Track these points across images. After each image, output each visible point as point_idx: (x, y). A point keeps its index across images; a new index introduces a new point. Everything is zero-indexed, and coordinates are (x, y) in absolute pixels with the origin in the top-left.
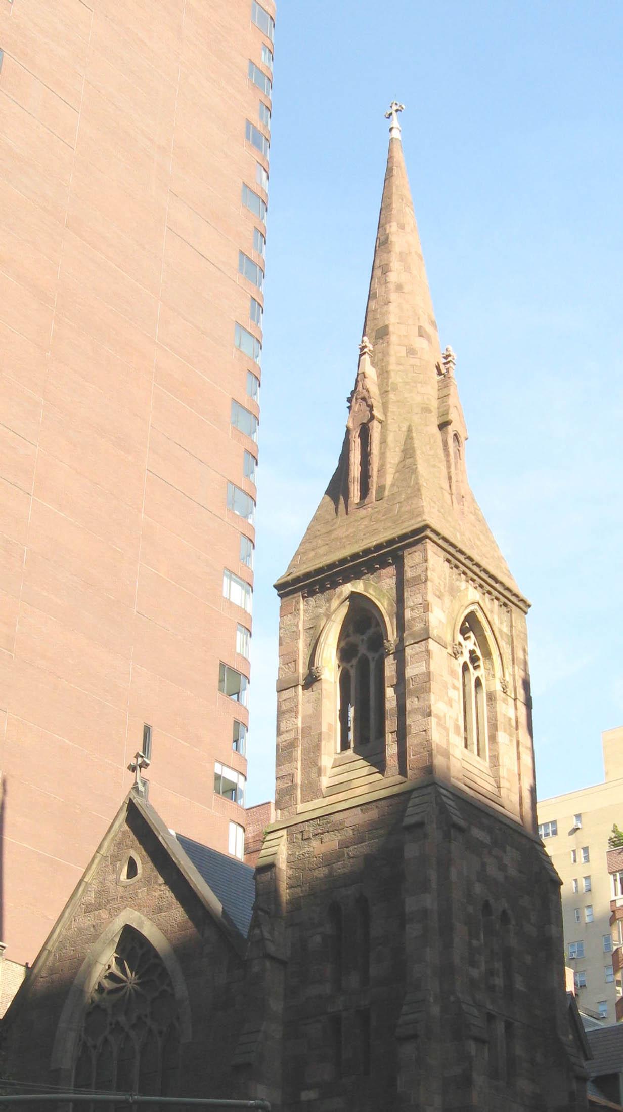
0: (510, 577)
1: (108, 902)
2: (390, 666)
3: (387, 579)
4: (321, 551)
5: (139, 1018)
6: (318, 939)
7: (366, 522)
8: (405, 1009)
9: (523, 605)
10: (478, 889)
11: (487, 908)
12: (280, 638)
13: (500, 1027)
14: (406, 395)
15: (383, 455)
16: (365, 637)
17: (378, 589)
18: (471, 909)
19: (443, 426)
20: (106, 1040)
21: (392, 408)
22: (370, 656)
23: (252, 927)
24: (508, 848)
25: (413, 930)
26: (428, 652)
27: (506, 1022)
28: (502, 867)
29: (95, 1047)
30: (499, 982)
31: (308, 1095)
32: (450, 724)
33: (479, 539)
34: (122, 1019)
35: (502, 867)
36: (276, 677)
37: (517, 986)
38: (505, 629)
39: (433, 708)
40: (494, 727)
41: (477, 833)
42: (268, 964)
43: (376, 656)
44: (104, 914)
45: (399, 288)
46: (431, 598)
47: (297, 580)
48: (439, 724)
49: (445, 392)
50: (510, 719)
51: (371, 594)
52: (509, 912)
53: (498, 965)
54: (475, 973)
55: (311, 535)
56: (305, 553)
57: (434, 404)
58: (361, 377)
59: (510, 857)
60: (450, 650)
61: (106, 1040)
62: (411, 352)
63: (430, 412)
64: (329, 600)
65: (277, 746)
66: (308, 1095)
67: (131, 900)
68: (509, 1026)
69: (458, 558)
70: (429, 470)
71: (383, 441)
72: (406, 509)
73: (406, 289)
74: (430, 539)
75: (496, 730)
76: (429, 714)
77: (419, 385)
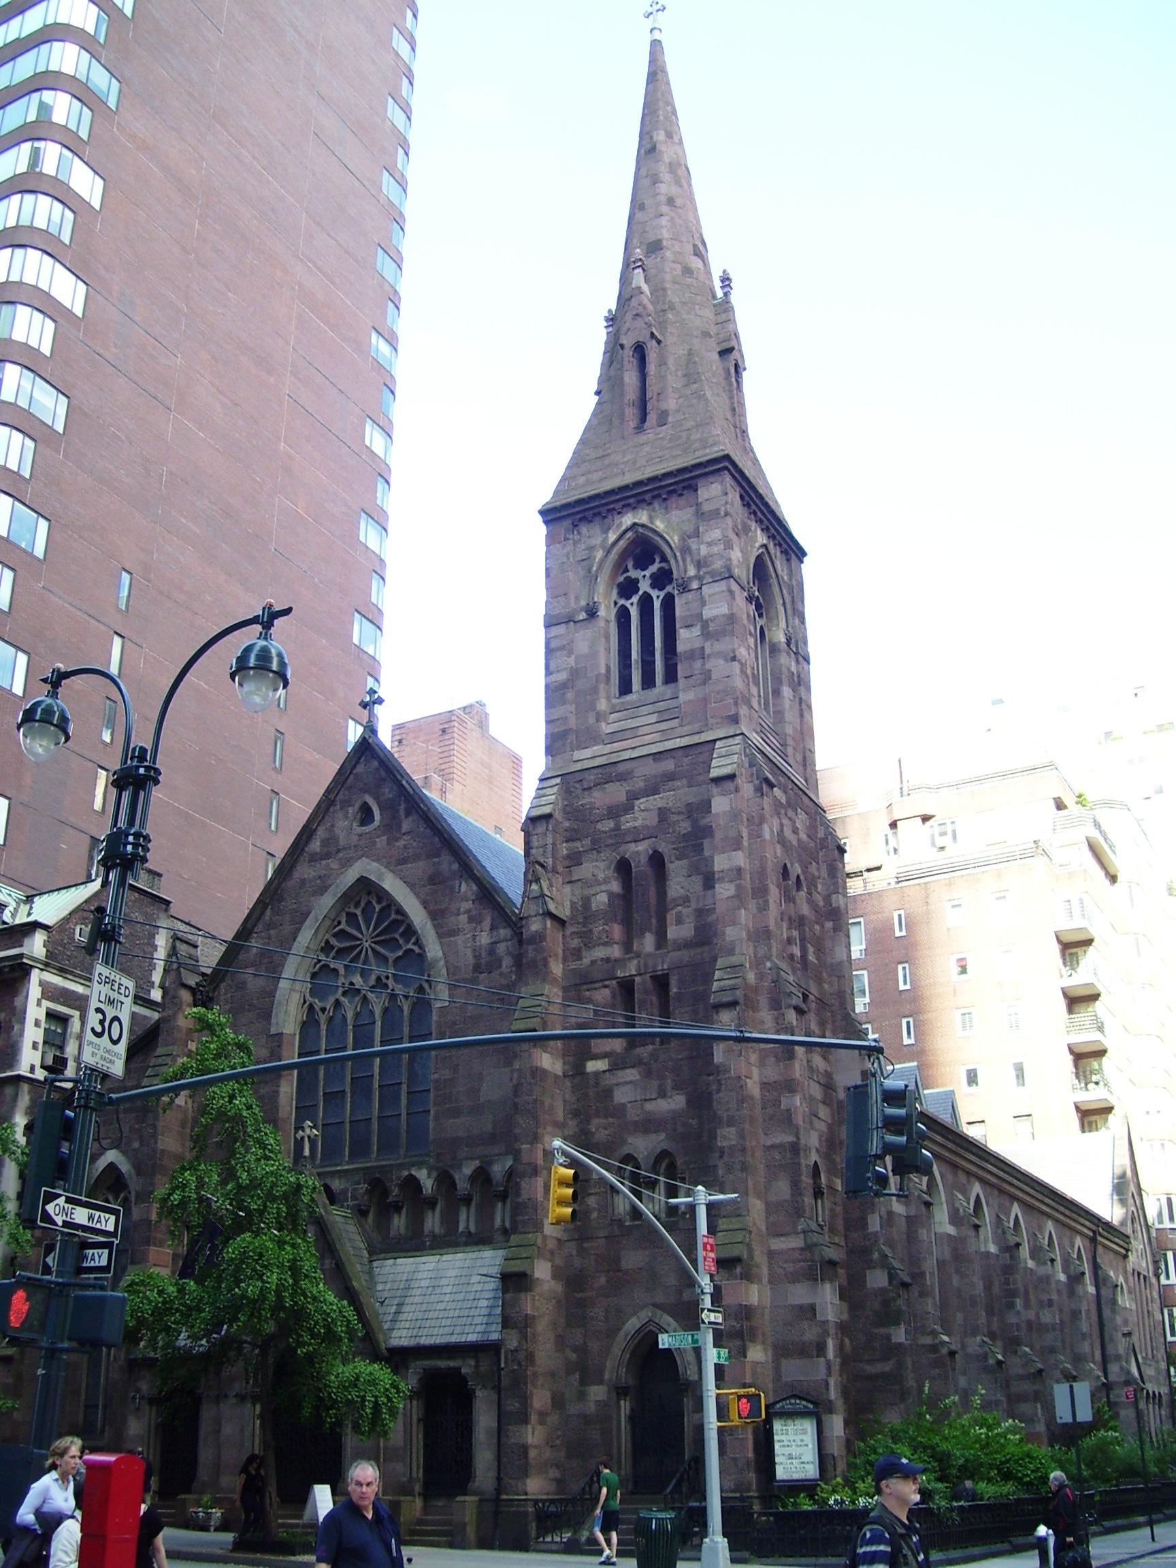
1: (339, 851)
4: (596, 476)
5: (379, 979)
6: (603, 898)
7: (647, 449)
8: (717, 975)
9: (800, 554)
12: (547, 569)
14: (684, 316)
16: (647, 573)
17: (666, 523)
19: (726, 352)
20: (338, 1004)
22: (654, 593)
25: (724, 890)
28: (795, 831)
29: (323, 1010)
30: (797, 951)
31: (592, 1066)
34: (358, 980)
35: (795, 831)
36: (542, 611)
42: (549, 923)
44: (334, 864)
45: (671, 201)
47: (567, 506)
49: (724, 317)
51: (659, 525)
52: (802, 877)
53: (795, 933)
55: (578, 460)
56: (574, 478)
61: (338, 1004)
63: (711, 337)
64: (606, 531)
65: (547, 687)
66: (592, 1066)
67: (365, 849)
72: (698, 436)
73: (678, 202)
74: (729, 470)
75: (781, 683)
77: (697, 307)
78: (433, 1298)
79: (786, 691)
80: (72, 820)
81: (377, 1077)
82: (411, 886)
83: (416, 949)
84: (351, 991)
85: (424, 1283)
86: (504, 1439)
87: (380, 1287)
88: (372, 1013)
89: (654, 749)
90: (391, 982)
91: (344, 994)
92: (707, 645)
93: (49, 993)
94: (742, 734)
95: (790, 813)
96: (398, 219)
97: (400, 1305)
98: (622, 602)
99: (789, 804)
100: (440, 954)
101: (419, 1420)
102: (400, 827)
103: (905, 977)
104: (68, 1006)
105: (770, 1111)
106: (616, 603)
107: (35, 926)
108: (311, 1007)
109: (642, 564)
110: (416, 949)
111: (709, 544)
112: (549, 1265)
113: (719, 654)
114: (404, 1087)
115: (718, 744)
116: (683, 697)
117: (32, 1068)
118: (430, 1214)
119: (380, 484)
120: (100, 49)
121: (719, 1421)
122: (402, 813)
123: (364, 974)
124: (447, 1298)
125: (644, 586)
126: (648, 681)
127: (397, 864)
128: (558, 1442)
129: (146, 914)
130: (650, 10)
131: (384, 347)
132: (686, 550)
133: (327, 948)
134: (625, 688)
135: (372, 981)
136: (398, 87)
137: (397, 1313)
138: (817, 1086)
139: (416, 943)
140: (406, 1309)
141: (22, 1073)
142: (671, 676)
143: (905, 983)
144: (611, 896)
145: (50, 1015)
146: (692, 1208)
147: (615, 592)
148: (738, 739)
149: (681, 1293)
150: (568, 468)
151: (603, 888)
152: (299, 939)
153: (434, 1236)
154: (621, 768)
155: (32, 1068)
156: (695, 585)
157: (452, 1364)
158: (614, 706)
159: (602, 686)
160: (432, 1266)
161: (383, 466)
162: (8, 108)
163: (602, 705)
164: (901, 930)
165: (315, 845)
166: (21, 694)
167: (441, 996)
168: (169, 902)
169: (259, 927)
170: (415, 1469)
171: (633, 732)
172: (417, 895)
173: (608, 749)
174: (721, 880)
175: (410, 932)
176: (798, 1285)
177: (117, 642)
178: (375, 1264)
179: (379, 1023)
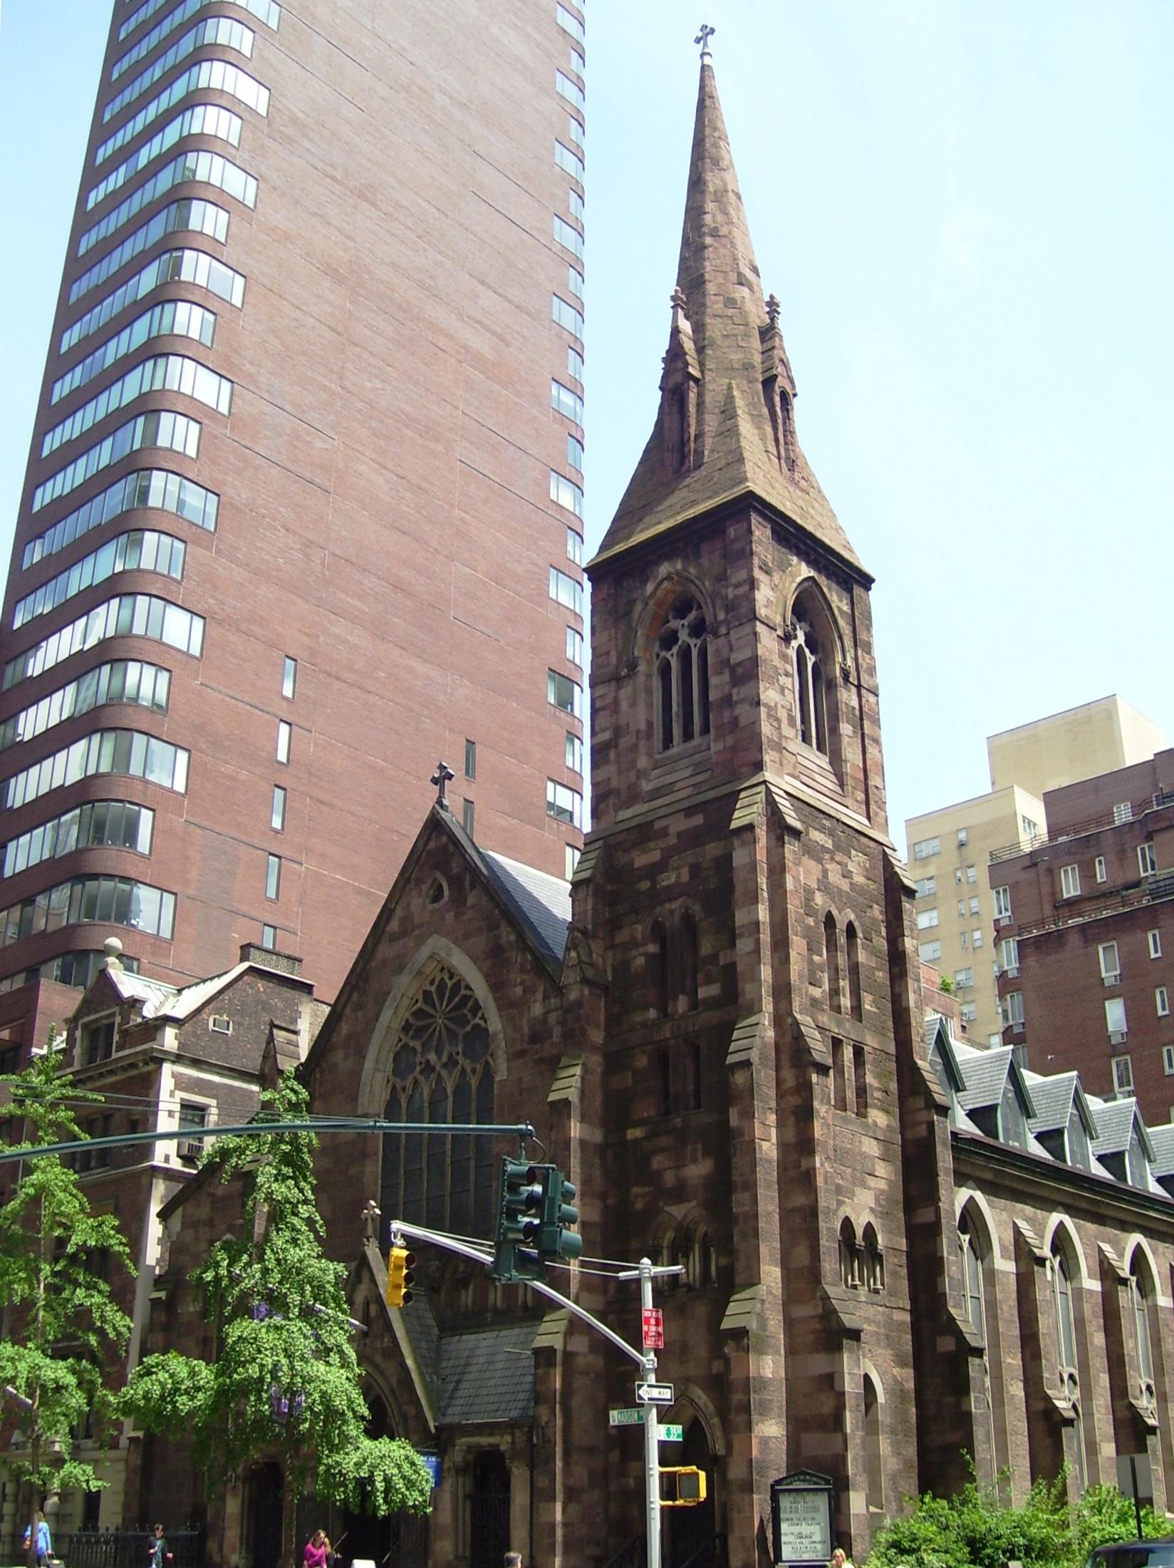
0: (850, 550)
1: (413, 930)
2: (1162, 884)
3: (710, 558)
5: (450, 1056)
6: (641, 961)
9: (866, 581)
10: (819, 898)
11: (830, 921)
13: (848, 1053)
15: (700, 422)
16: (686, 622)
18: (811, 921)
19: (769, 382)
20: (416, 1082)
21: (710, 365)
22: (692, 642)
23: (568, 949)
24: (853, 852)
26: (755, 633)
27: (854, 1046)
28: (847, 875)
30: (846, 1002)
31: (634, 1133)
32: (782, 714)
33: (813, 508)
34: (432, 1057)
37: (867, 1007)
38: (846, 608)
39: (762, 697)
40: (835, 719)
41: (816, 836)
43: (699, 642)
46: (757, 573)
48: (769, 716)
50: (854, 708)
52: (856, 924)
54: (816, 992)
57: (757, 359)
58: (675, 332)
59: (856, 862)
60: (780, 632)
62: (730, 302)
66: (634, 1133)
68: (858, 1052)
69: (795, 538)
70: (752, 437)
71: (700, 404)
76: (758, 703)
78: (487, 1375)
79: (846, 729)
80: (244, 909)
81: (449, 1153)
82: (474, 959)
83: (482, 1022)
84: (428, 1068)
85: (482, 1360)
86: (535, 1516)
87: (444, 1364)
88: (445, 1089)
89: (686, 804)
90: (460, 1058)
91: (422, 1072)
92: (735, 691)
93: (181, 1083)
94: (765, 782)
95: (839, 857)
96: (577, 265)
97: (458, 1382)
98: (663, 654)
99: (837, 847)
100: (500, 1027)
101: (466, 1497)
102: (465, 900)
103: (1163, 1001)
104: (204, 1095)
105: (792, 1173)
106: (658, 656)
107: (167, 1020)
108: (394, 1087)
109: (681, 612)
110: (482, 1022)
111: (736, 586)
112: (587, 1338)
113: (743, 701)
114: (472, 1163)
115: (742, 795)
116: (715, 747)
117: (167, 1159)
118: (463, 1291)
119: (571, 538)
120: (233, 151)
121: (662, 1498)
122: (467, 884)
123: (439, 1053)
124: (499, 1374)
125: (683, 636)
126: (688, 736)
127: (461, 940)
128: (597, 1519)
129: (286, 1000)
130: (700, 34)
131: (567, 398)
132: (714, 595)
133: (406, 1028)
134: (668, 742)
135: (445, 1059)
136: (566, 131)
137: (455, 1389)
138: (875, 1142)
139: (483, 1018)
140: (462, 1386)
141: (155, 1163)
142: (705, 730)
143: (1164, 1009)
144: (648, 956)
145: (186, 1106)
146: (638, 1282)
147: (657, 644)
148: (762, 788)
149: (710, 1367)
150: (613, 522)
151: (641, 950)
152: (381, 1019)
153: (496, 1311)
154: (657, 825)
155: (167, 1159)
156: (723, 630)
157: (492, 1440)
158: (656, 762)
159: (642, 743)
160: (490, 1342)
161: (573, 518)
162: (152, 223)
163: (643, 762)
164: (1156, 952)
165: (394, 925)
166: (183, 791)
167: (502, 1072)
168: (312, 986)
169: (348, 1010)
170: (460, 1545)
171: (669, 788)
172: (480, 968)
173: (646, 807)
174: (741, 935)
175: (477, 1007)
176: (816, 1356)
177: (284, 730)
178: (444, 1341)
179: (451, 1099)
